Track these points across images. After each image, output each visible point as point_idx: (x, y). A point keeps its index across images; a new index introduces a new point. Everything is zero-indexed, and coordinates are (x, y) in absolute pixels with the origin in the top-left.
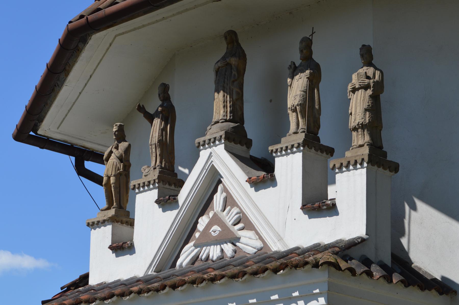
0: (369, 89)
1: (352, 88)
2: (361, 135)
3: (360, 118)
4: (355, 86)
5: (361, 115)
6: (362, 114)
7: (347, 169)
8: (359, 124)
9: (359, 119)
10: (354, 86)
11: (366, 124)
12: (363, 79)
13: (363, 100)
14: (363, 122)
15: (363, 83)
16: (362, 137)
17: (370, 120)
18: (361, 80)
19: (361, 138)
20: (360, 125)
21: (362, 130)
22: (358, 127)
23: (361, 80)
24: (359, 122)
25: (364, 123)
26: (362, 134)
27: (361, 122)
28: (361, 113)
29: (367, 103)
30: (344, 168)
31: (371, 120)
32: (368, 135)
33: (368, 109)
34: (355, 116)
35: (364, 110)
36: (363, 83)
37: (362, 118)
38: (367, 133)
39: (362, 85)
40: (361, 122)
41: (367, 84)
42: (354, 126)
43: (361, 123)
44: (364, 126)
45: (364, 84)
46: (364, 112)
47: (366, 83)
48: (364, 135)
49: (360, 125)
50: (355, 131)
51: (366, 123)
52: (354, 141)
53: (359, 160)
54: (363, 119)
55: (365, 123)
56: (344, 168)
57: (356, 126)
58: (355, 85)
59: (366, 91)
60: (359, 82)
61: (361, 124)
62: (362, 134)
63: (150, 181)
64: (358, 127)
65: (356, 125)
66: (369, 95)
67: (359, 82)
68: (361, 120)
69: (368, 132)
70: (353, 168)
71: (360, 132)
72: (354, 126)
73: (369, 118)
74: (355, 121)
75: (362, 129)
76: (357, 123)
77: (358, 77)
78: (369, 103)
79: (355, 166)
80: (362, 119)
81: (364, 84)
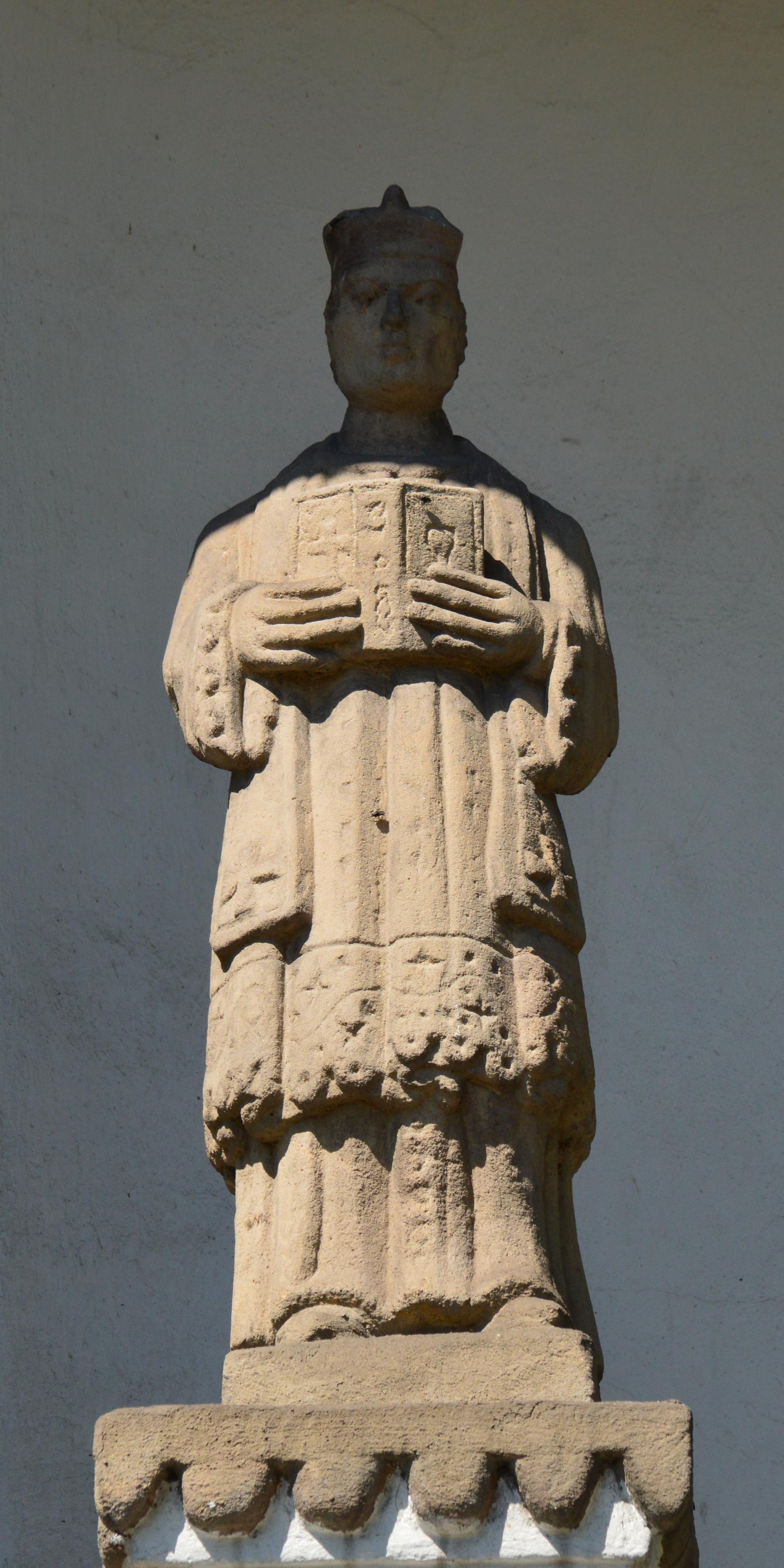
0: (517, 704)
1: (311, 645)
2: (430, 1194)
3: (453, 997)
4: (359, 632)
5: (453, 970)
6: (469, 956)
7: (349, 1541)
8: (439, 1059)
9: (430, 1003)
10: (346, 623)
11: (517, 1083)
12: (460, 566)
13: (470, 804)
14: (482, 1050)
15: (465, 609)
16: (442, 1217)
17: (559, 1050)
18: (440, 578)
19: (434, 1227)
20: (447, 1082)
21: (453, 1148)
22: (402, 1095)
23: (440, 578)
24: (434, 1042)
25: (492, 1060)
26: (443, 1188)
27: (460, 1041)
28: (458, 947)
29: (520, 846)
30: (297, 1527)
31: (567, 1050)
32: (515, 1205)
33: (540, 916)
34: (365, 957)
35: (486, 926)
36: (465, 609)
37: (471, 998)
38: (506, 1184)
39: (459, 632)
40: (460, 1041)
41: (515, 637)
42: (359, 1076)
43: (465, 1052)
44: (482, 1095)
45: (476, 623)
46: (486, 941)
47: (505, 628)
48: (468, 1201)
49: (447, 1082)
50: (350, 1142)
51: (511, 1071)
52: (317, 1246)
53: (555, 1468)
54: (487, 1020)
55: (506, 1062)
56: (297, 1527)
57: (377, 1078)
58: (355, 610)
59: (487, 716)
60: (419, 596)
61: (454, 1067)
62: (443, 1188)
63: (552, 1323)
64: (402, 1095)
65: (386, 1061)
66: (528, 761)
67: (419, 596)
68: (464, 1020)
69: (518, 1179)
70: (443, 1542)
71: (429, 1161)
72: (355, 1069)
73: (549, 1019)
74: (370, 1020)
75: (447, 1136)
76: (417, 1048)
77: (403, 526)
78: (540, 854)
79: (472, 1527)
80: (476, 1009)
81: (476, 623)
